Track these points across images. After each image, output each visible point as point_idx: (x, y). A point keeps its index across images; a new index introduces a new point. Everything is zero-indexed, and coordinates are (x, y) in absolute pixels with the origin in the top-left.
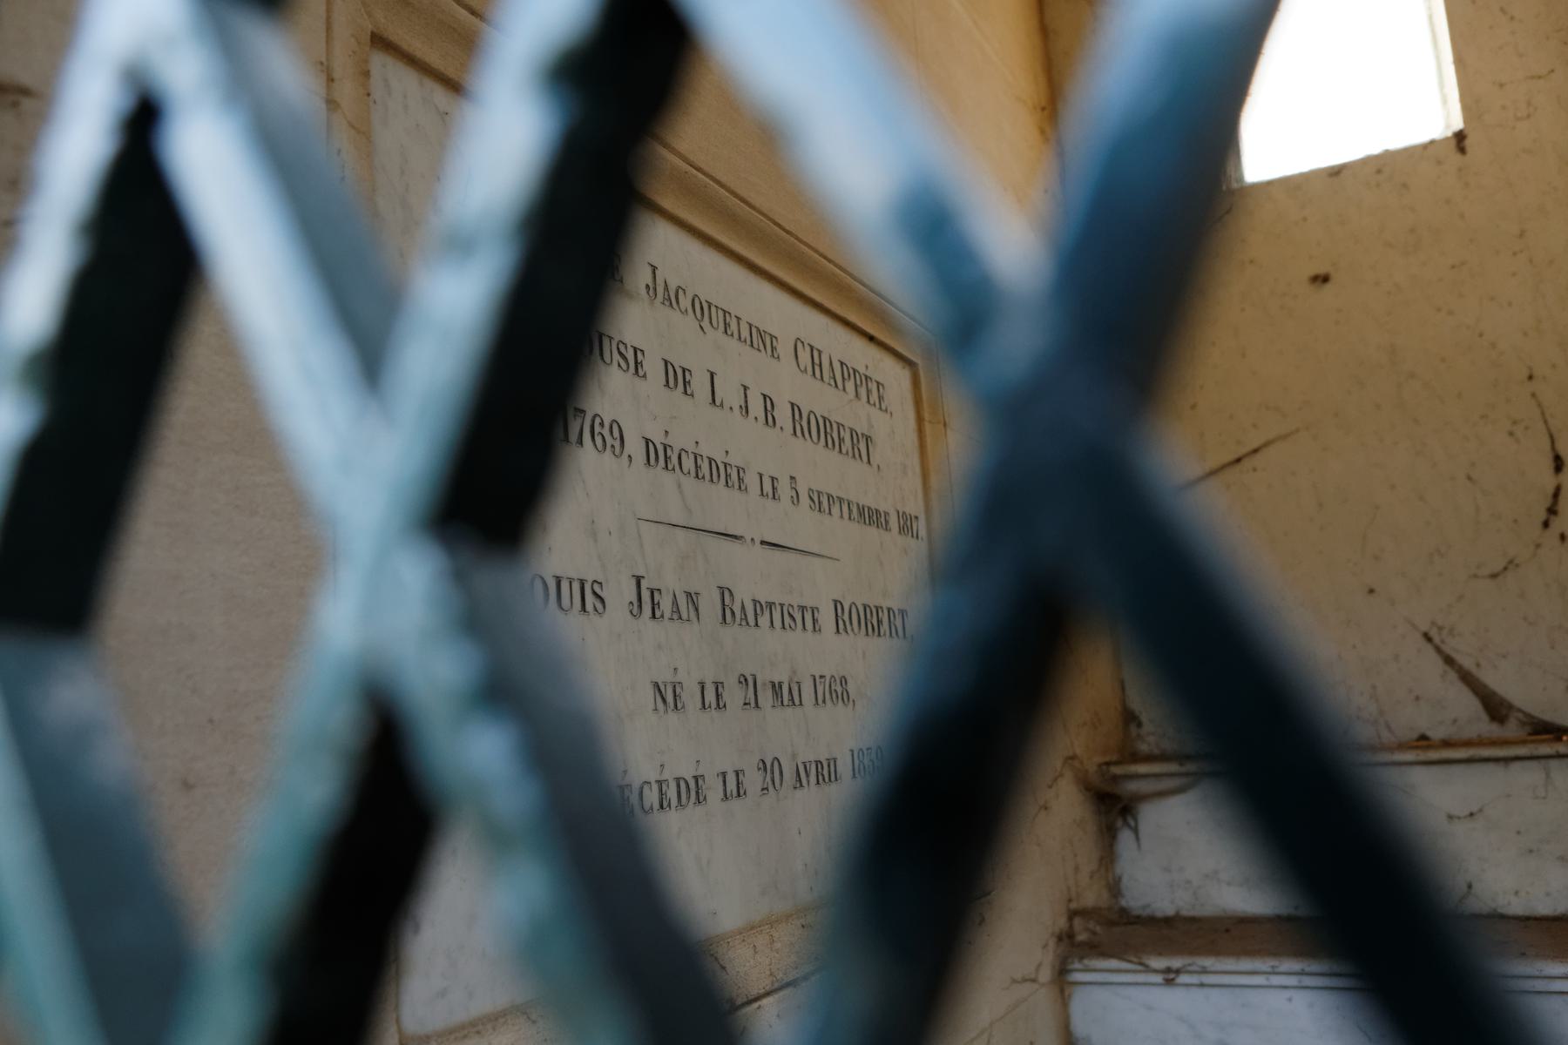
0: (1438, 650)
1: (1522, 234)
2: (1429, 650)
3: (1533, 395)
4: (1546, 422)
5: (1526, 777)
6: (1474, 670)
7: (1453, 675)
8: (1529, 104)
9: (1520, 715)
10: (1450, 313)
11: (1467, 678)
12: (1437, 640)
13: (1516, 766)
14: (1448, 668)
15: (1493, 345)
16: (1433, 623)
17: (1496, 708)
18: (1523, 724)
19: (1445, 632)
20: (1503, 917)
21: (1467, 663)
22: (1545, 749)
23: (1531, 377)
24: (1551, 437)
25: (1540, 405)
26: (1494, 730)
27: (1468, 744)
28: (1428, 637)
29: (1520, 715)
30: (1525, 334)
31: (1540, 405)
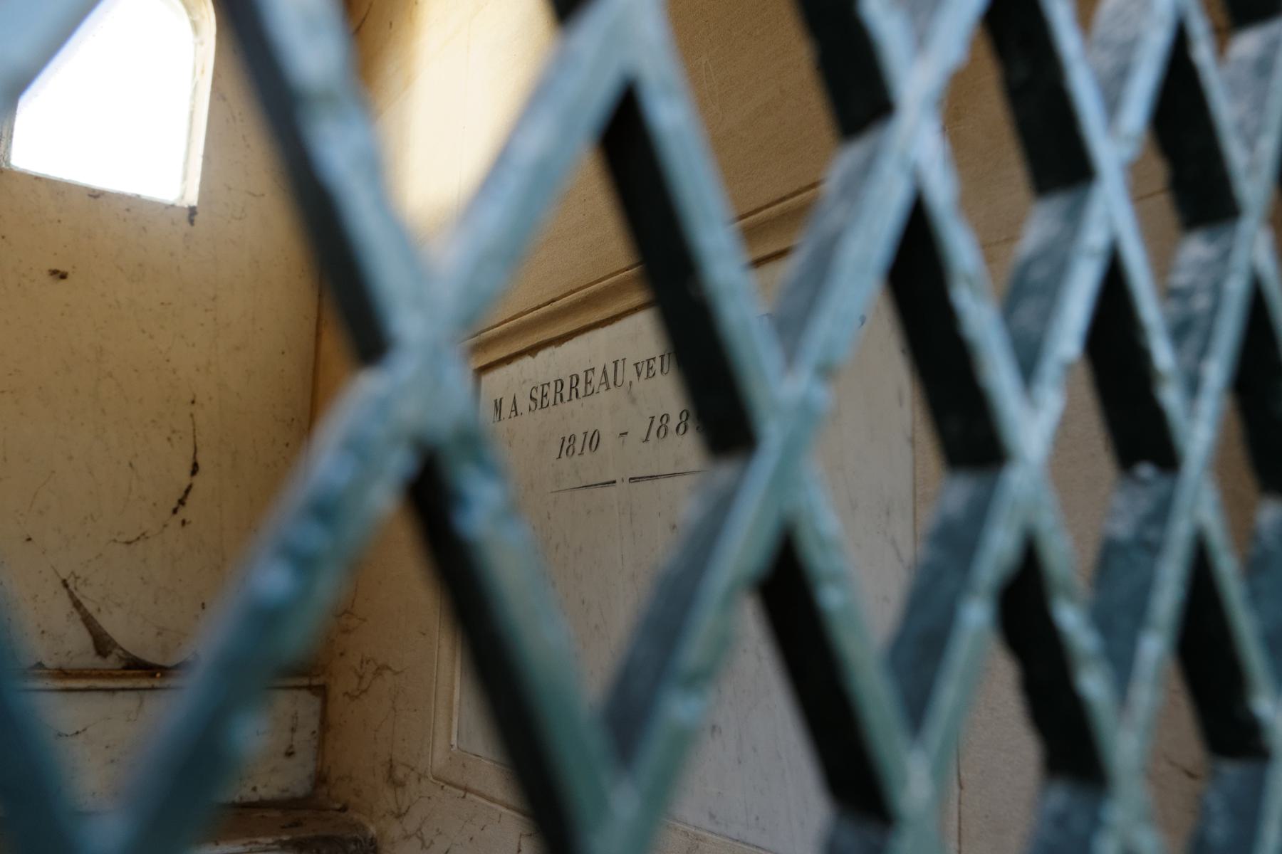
0: (71, 595)
1: (214, 299)
2: (65, 592)
3: (192, 415)
5: (124, 703)
7: (77, 616)
11: (88, 620)
12: (71, 587)
14: (74, 610)
15: (174, 372)
17: (102, 644)
18: (121, 658)
19: (79, 581)
21: (90, 607)
22: (145, 683)
23: (193, 402)
25: (194, 424)
26: (98, 662)
27: (80, 674)
29: (120, 652)
31: (194, 424)
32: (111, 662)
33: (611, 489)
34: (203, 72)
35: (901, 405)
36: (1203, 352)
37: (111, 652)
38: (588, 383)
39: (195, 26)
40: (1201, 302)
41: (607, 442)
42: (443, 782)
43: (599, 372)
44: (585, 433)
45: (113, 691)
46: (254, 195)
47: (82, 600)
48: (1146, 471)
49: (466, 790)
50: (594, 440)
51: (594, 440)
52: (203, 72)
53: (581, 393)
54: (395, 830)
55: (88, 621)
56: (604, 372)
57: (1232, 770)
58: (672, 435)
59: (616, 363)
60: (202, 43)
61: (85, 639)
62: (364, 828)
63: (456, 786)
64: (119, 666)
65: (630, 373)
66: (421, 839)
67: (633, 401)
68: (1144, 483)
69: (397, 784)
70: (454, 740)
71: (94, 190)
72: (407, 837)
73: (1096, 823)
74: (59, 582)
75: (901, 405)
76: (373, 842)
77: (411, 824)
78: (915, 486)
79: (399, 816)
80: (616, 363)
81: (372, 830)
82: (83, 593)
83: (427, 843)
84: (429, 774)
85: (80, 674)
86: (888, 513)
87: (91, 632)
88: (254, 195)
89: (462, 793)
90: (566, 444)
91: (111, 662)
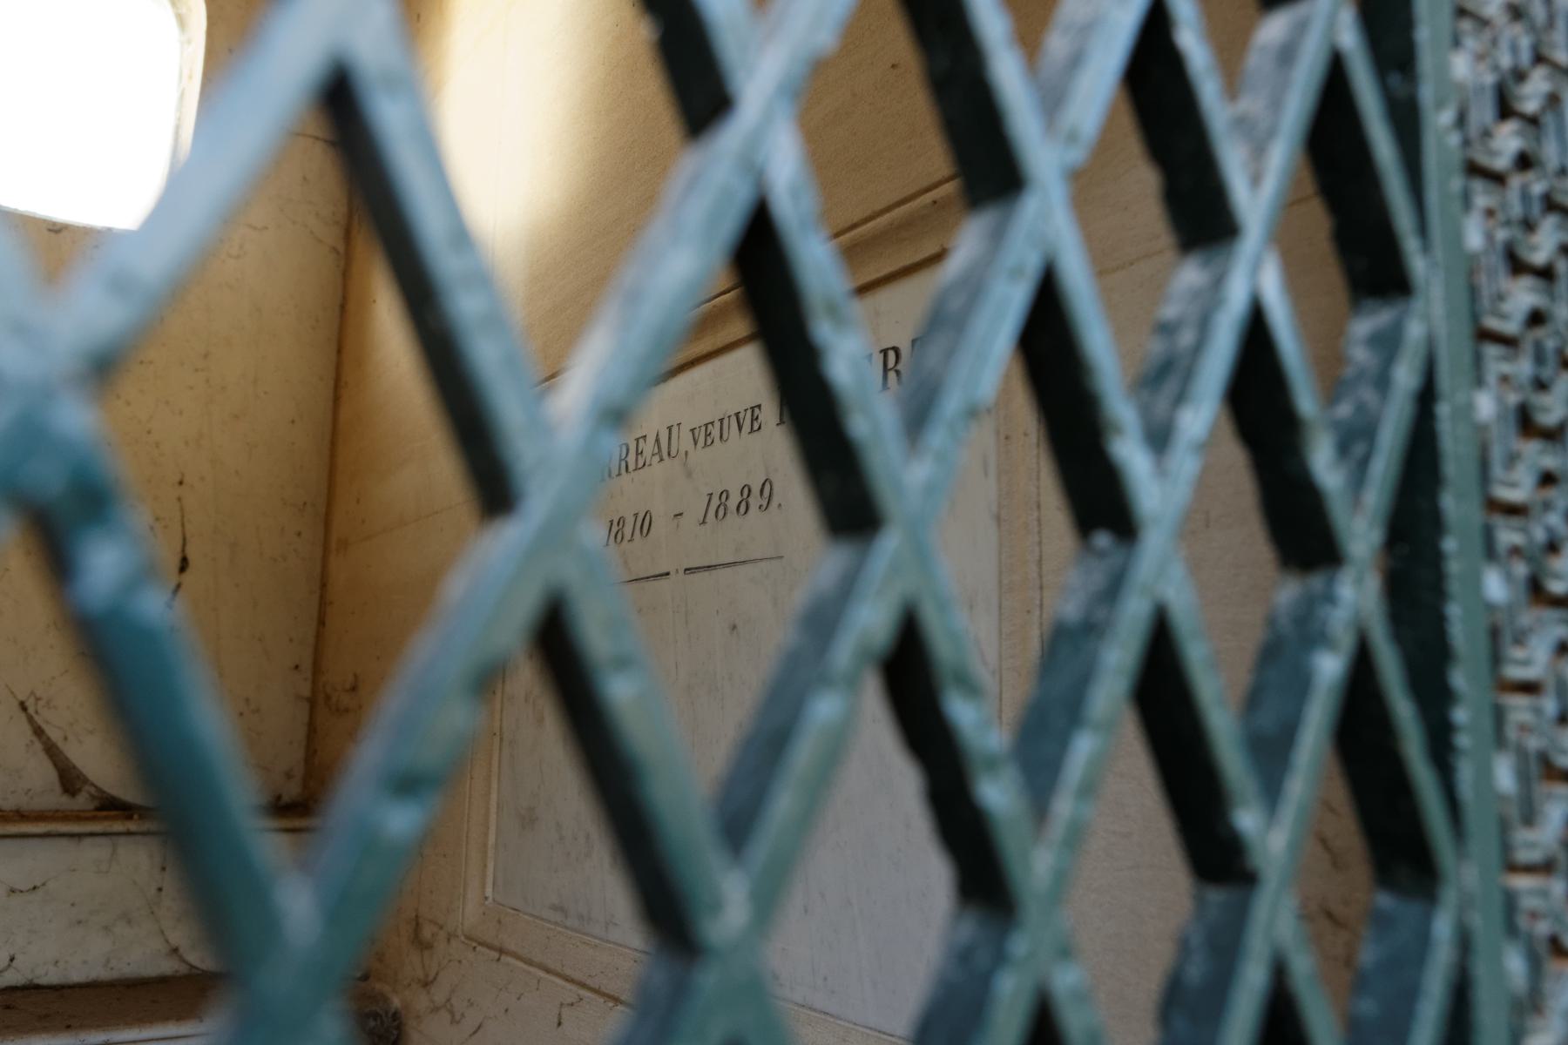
0: (31, 720)
1: (206, 356)
2: (23, 716)
3: (179, 499)
4: (183, 525)
5: (93, 851)
6: (60, 744)
7: (38, 746)
8: (241, 247)
9: (93, 790)
10: (128, 404)
11: (52, 751)
12: (31, 710)
13: (88, 841)
14: (34, 738)
15: (157, 445)
16: (32, 693)
17: (70, 779)
18: (93, 797)
19: (41, 703)
20: (38, 987)
21: (54, 734)
22: (118, 826)
23: (181, 483)
24: (184, 539)
25: (182, 509)
26: (65, 802)
27: (40, 817)
28: (23, 707)
29: (93, 790)
30: (187, 443)
31: (182, 509)
32: (82, 802)
33: (663, 582)
34: (190, 77)
35: (986, 474)
36: (1180, 398)
37: (80, 790)
38: (639, 453)
39: (182, 21)
40: (1186, 338)
41: (660, 526)
42: (475, 942)
43: (651, 439)
44: (636, 515)
45: (79, 836)
46: (255, 228)
47: (44, 726)
48: (1102, 539)
49: (501, 951)
50: (645, 523)
51: (645, 523)
52: (190, 77)
53: (631, 467)
54: (421, 1002)
55: (52, 751)
56: (657, 440)
57: (1217, 896)
58: (732, 517)
59: (670, 428)
60: (189, 42)
61: (52, 775)
62: (386, 999)
63: (490, 947)
64: (91, 806)
65: (686, 437)
66: (452, 1013)
67: (689, 475)
68: (1101, 555)
69: (423, 946)
70: (489, 892)
71: (54, 224)
72: (436, 1010)
73: (1000, 958)
74: (16, 704)
75: (986, 474)
76: (396, 1016)
77: (439, 995)
78: (1000, 573)
79: (426, 984)
80: (670, 428)
81: (396, 1002)
82: (46, 718)
83: (458, 1017)
84: (459, 932)
85: (40, 817)
86: (971, 607)
87: (55, 765)
88: (255, 228)
89: (495, 955)
90: (615, 529)
91: (82, 802)
